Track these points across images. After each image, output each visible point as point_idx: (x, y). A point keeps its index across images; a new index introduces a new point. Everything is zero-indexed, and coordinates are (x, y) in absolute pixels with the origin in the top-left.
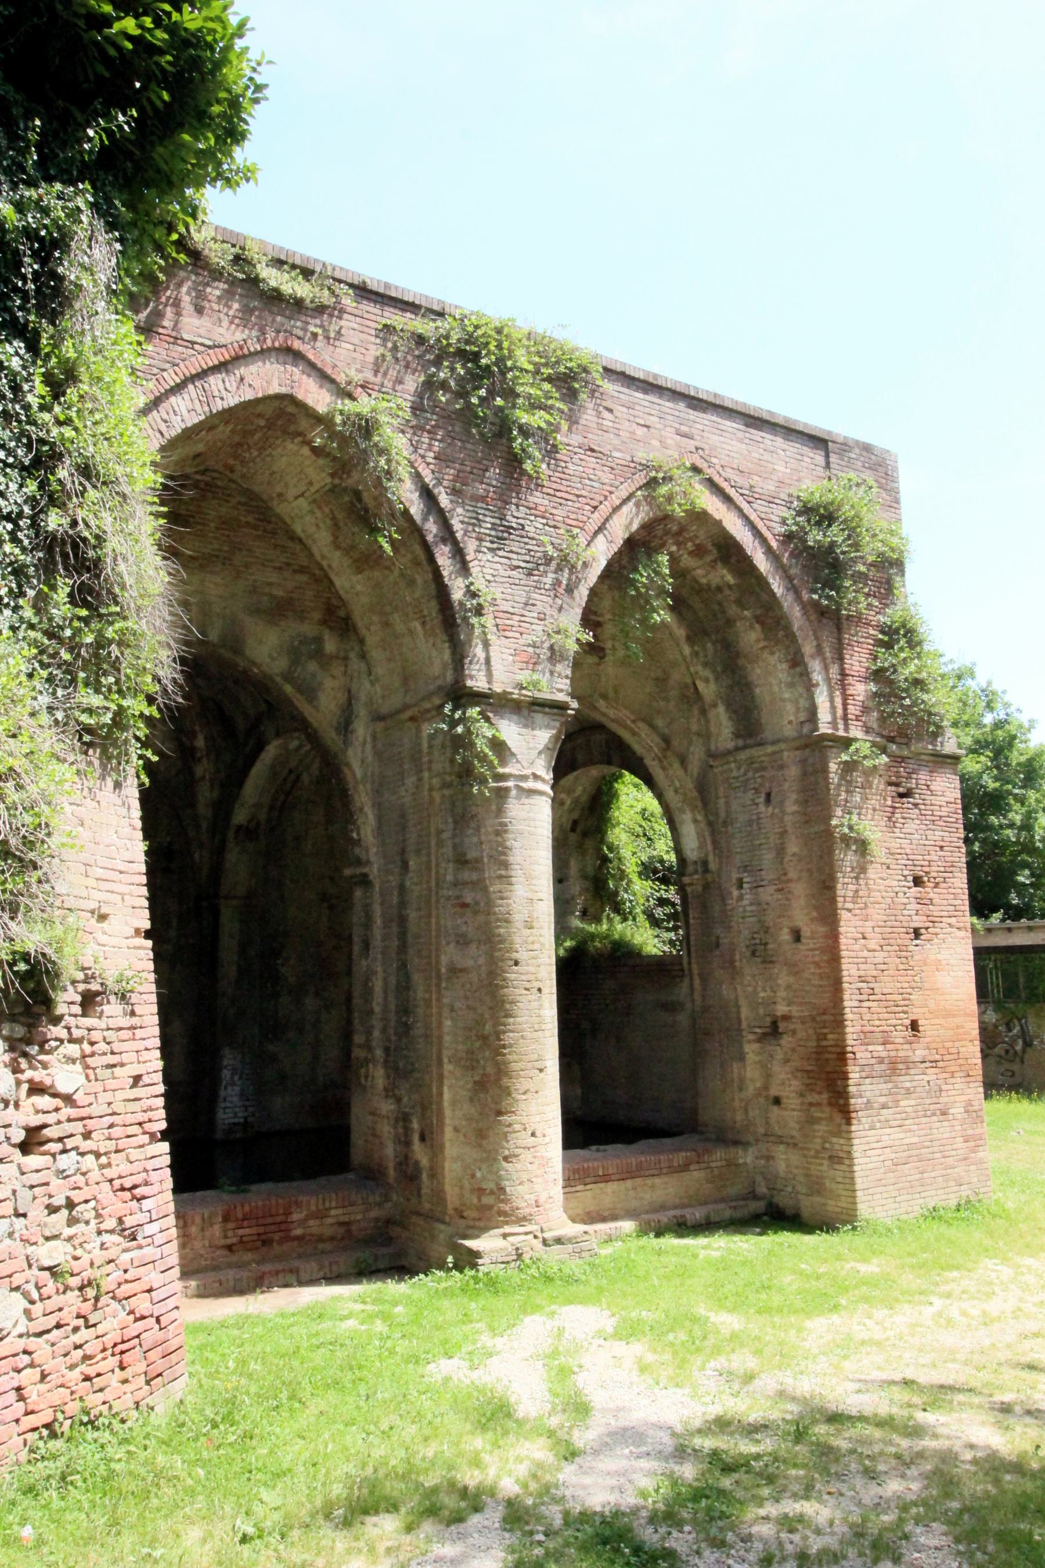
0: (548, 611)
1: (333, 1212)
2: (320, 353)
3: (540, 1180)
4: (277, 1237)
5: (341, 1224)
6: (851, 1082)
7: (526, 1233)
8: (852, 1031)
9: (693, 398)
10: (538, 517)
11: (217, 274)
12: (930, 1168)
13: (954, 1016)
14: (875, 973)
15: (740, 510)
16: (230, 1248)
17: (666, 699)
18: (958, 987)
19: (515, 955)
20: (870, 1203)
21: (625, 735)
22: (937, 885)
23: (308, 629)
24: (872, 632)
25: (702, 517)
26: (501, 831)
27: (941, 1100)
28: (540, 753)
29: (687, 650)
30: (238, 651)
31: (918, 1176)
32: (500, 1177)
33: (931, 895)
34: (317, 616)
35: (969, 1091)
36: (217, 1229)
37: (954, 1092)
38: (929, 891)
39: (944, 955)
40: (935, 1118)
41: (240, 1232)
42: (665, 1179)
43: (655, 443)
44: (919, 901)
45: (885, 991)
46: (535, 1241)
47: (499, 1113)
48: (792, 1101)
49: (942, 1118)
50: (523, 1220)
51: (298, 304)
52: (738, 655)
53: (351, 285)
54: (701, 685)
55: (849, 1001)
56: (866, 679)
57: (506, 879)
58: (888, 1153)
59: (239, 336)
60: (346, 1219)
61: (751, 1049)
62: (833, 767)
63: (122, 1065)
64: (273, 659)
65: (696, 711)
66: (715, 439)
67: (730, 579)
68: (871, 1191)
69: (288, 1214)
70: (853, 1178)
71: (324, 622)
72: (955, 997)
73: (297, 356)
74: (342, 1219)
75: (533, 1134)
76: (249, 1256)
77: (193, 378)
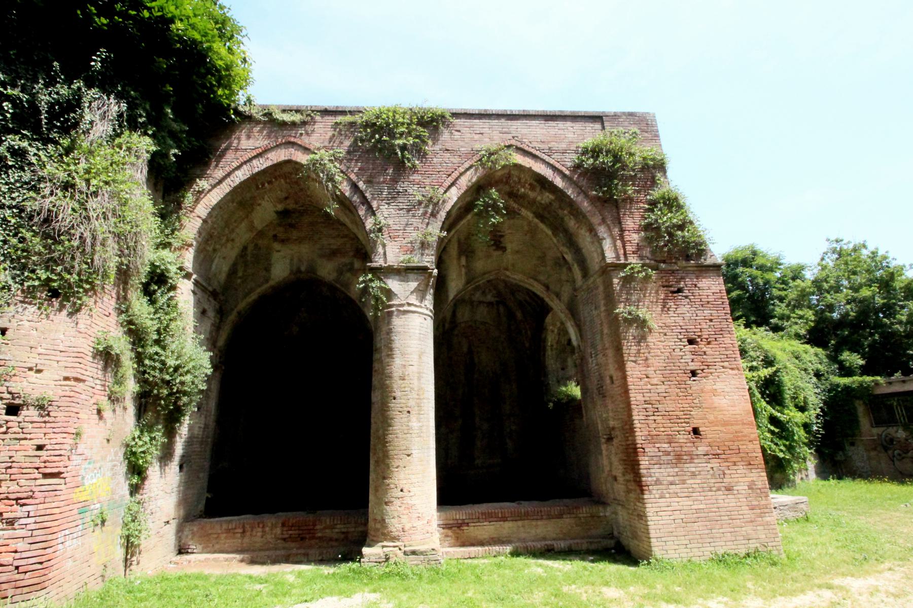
0: (420, 226)
1: (338, 526)
2: (305, 141)
3: (405, 517)
4: (307, 536)
5: (343, 533)
6: (641, 467)
7: (394, 547)
8: (640, 436)
9: (510, 115)
10: (415, 187)
11: (258, 122)
12: (717, 527)
13: (732, 425)
14: (658, 398)
15: (544, 161)
16: (284, 539)
17: (545, 266)
18: (734, 406)
19: (394, 394)
20: (657, 549)
21: (531, 288)
22: (709, 343)
23: (346, 260)
24: (642, 205)
25: (518, 167)
26: (389, 332)
27: (725, 480)
28: (412, 292)
29: (555, 240)
30: (315, 273)
31: (707, 532)
32: (383, 513)
33: (705, 349)
34: (351, 254)
35: (752, 475)
36: (278, 531)
37: (737, 475)
38: (703, 346)
39: (719, 386)
40: (720, 493)
41: (290, 532)
42: (545, 522)
43: (487, 140)
44: (694, 353)
45: (667, 409)
46: (399, 552)
47: (384, 478)
48: (621, 479)
49: (727, 492)
50: (394, 539)
51: (294, 124)
52: (571, 235)
53: (318, 111)
54: (566, 256)
55: (637, 417)
56: (638, 231)
57: (391, 356)
58: (677, 515)
59: (266, 142)
60: (345, 530)
61: (604, 447)
62: (616, 281)
63: (30, 439)
64: (329, 274)
65: (564, 270)
66: (525, 131)
67: (552, 197)
68: (663, 539)
69: (314, 525)
70: (648, 530)
71: (355, 256)
72: (731, 412)
73: (293, 144)
74: (343, 530)
75: (402, 491)
76: (293, 545)
77: (245, 163)
